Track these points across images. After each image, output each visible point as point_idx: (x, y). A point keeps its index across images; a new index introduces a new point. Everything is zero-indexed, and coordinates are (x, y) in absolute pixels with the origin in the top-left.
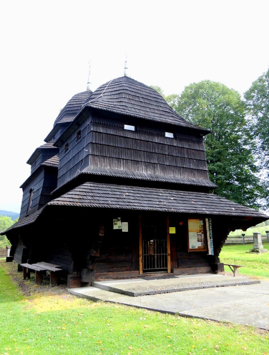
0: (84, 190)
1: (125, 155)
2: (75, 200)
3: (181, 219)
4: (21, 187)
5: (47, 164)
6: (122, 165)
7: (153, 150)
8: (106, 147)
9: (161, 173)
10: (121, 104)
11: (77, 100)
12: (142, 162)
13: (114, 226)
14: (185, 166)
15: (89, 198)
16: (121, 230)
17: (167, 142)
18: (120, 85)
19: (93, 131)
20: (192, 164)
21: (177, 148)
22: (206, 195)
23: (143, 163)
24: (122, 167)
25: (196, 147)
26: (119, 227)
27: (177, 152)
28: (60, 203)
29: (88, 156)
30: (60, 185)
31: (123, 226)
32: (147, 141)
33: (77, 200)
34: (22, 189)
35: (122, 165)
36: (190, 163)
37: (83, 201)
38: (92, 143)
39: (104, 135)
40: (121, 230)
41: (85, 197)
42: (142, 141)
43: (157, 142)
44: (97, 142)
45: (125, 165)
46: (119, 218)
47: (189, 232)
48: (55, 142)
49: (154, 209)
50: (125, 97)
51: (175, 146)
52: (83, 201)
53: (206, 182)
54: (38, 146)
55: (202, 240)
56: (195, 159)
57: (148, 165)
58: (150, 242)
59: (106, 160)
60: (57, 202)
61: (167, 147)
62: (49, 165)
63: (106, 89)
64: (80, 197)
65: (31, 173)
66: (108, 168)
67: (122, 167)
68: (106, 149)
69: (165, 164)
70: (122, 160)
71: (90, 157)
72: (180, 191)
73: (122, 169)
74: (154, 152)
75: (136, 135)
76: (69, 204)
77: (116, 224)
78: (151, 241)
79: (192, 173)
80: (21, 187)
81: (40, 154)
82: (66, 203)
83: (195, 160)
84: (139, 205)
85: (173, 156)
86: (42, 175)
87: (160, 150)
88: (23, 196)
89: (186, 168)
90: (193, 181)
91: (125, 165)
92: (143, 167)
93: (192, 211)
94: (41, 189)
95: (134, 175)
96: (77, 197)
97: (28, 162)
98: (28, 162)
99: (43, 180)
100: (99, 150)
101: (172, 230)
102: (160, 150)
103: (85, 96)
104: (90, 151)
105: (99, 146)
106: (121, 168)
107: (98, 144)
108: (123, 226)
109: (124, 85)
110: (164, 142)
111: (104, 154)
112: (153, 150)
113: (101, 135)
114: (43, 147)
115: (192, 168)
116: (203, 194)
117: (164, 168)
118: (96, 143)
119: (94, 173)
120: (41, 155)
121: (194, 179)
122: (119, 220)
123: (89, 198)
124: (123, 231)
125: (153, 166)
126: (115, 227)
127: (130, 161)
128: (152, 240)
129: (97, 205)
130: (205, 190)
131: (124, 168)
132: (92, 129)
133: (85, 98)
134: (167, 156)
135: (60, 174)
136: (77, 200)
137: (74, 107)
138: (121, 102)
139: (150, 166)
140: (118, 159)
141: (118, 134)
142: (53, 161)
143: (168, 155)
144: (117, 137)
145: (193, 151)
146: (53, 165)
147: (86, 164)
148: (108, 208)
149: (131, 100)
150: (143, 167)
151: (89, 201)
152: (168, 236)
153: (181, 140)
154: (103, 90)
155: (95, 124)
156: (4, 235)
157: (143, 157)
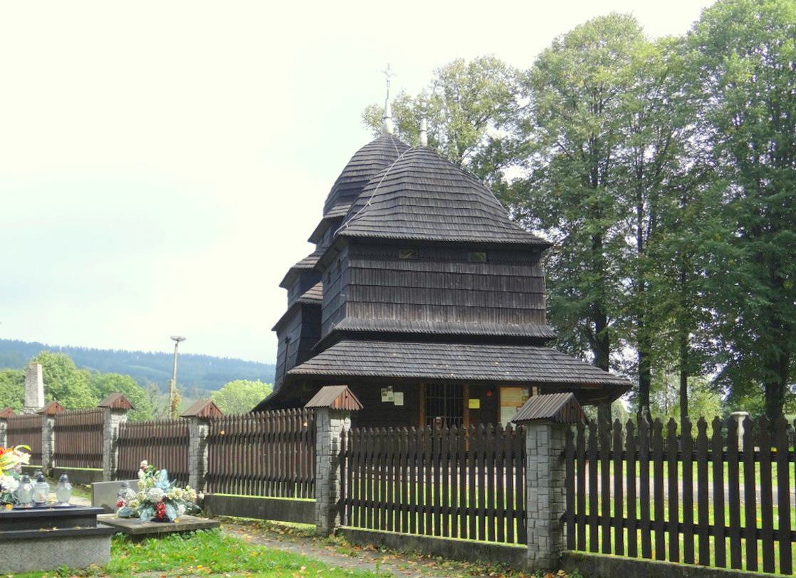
0: (336, 353)
1: (399, 296)
2: (319, 367)
3: (490, 390)
4: (273, 330)
5: (305, 301)
6: (394, 313)
7: (446, 284)
8: (371, 288)
9: (456, 320)
10: (396, 217)
11: (359, 168)
12: (426, 305)
13: (383, 397)
14: (501, 306)
15: (339, 363)
16: (393, 403)
17: (470, 269)
18: (399, 181)
19: (351, 268)
20: (514, 302)
21: (488, 277)
22: (533, 350)
23: (428, 306)
24: (394, 316)
25: (525, 271)
26: (390, 399)
27: (488, 284)
28: (302, 371)
29: (345, 303)
30: (324, 335)
31: (398, 399)
32: (436, 272)
33: (323, 367)
34: (275, 333)
35: (394, 313)
36: (511, 300)
37: (330, 367)
38: (350, 285)
39: (367, 271)
40: (393, 403)
41: (334, 363)
42: (427, 274)
43: (452, 271)
44: (357, 282)
45: (398, 312)
46: (390, 387)
47: (502, 407)
48: (316, 262)
49: (423, 375)
50: (404, 204)
51: (485, 275)
52: (330, 367)
53: (548, 330)
54: (292, 264)
55: (63, 402)
56: (522, 293)
57: (435, 309)
58: (436, 420)
59: (370, 307)
60: (298, 370)
61: (470, 278)
62: (309, 301)
63: (379, 188)
64: (328, 362)
65: (289, 304)
66: (374, 318)
67: (394, 316)
68: (371, 291)
69: (466, 305)
70: (394, 306)
71: (348, 305)
72: (488, 346)
73: (394, 319)
74: (446, 287)
75: (418, 264)
76: (311, 371)
77: (385, 395)
78: (437, 418)
79: (515, 317)
80: (273, 330)
81: (297, 279)
82: (308, 371)
83: (521, 295)
84: (404, 370)
85: (481, 291)
86: (299, 318)
87: (457, 284)
88: (279, 346)
89: (502, 308)
90: (513, 329)
91: (398, 312)
92: (428, 312)
93: (483, 377)
94: (299, 341)
95: (411, 326)
96: (324, 362)
97: (282, 285)
98: (282, 285)
99: (300, 327)
100: (361, 294)
101: (474, 404)
102: (457, 284)
103: (373, 157)
104: (348, 296)
105: (361, 288)
106: (392, 317)
107: (359, 285)
108: (398, 399)
109: (405, 181)
110: (466, 270)
111: (368, 299)
112: (446, 284)
113: (363, 271)
114: (301, 266)
115: (514, 307)
116: (530, 348)
117: (463, 312)
118: (356, 285)
119: (351, 328)
120: (298, 280)
121: (517, 325)
122: (389, 390)
123: (339, 363)
124: (396, 404)
125: (445, 310)
126: (385, 399)
127: (408, 306)
128: (438, 416)
129: (346, 372)
130: (539, 342)
131: (397, 317)
132: (349, 265)
133: (372, 162)
134: (471, 292)
135: (325, 316)
136: (323, 367)
137: (354, 182)
138: (395, 214)
139: (440, 309)
140: (389, 304)
141: (388, 268)
142: (316, 292)
143: (473, 290)
144: (387, 272)
145: (519, 280)
146: (315, 302)
147: (343, 316)
148: (359, 376)
149: (414, 208)
150: (428, 312)
151: (337, 367)
152: (466, 414)
153: (496, 263)
154: (372, 189)
155: (353, 257)
156: (686, 379)
157: (428, 298)
